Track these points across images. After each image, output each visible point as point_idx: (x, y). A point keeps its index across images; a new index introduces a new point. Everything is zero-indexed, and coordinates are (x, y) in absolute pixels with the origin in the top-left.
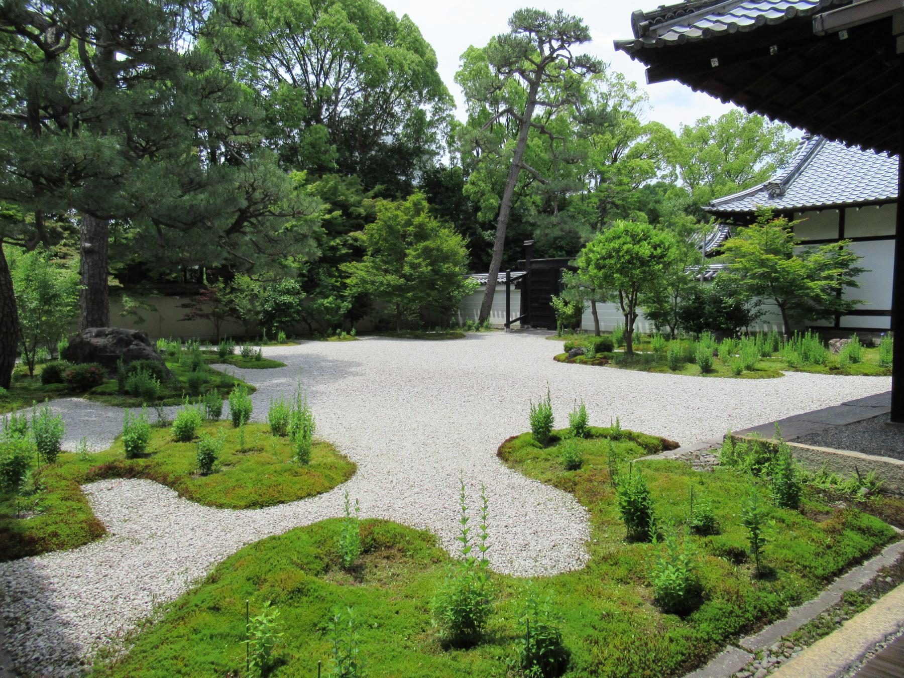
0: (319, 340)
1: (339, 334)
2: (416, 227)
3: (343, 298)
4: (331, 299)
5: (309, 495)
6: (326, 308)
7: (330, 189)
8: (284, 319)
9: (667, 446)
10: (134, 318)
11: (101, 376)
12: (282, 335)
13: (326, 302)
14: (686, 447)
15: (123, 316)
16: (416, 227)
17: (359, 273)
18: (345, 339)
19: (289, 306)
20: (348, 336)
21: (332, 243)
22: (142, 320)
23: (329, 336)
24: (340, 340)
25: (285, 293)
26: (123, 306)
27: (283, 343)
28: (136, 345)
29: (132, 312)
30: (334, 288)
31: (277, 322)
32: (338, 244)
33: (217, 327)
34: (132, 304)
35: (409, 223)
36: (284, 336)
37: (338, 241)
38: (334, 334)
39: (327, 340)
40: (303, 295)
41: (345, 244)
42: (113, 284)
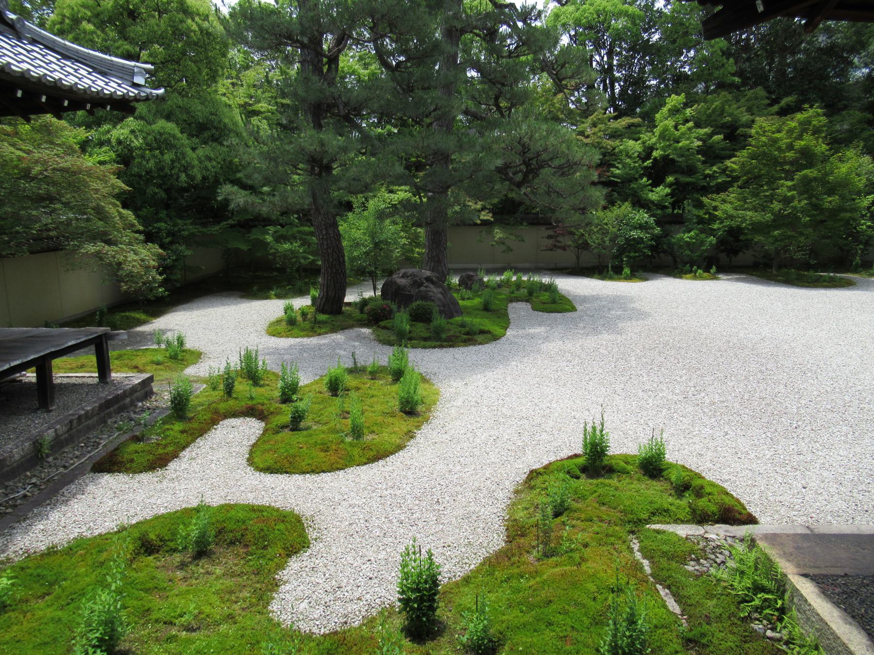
0: (675, 277)
1: (695, 272)
2: (797, 151)
3: (712, 232)
4: (692, 233)
5: (313, 472)
6: (688, 243)
7: (714, 110)
8: (632, 254)
9: (732, 514)
10: (504, 248)
11: (391, 312)
12: (627, 271)
13: (686, 237)
14: (767, 524)
15: (493, 245)
16: (797, 151)
17: (728, 207)
18: (701, 278)
19: (640, 240)
20: (706, 274)
21: (708, 172)
22: (510, 249)
23: (686, 273)
24: (695, 278)
25: (636, 228)
26: (494, 237)
27: (628, 278)
28: (426, 287)
29: (501, 242)
30: (701, 221)
31: (626, 257)
32: (715, 172)
33: (578, 258)
34: (501, 235)
35: (790, 147)
36: (629, 272)
37: (715, 168)
38: (691, 272)
39: (681, 278)
40: (658, 230)
41: (724, 171)
42: (485, 218)
